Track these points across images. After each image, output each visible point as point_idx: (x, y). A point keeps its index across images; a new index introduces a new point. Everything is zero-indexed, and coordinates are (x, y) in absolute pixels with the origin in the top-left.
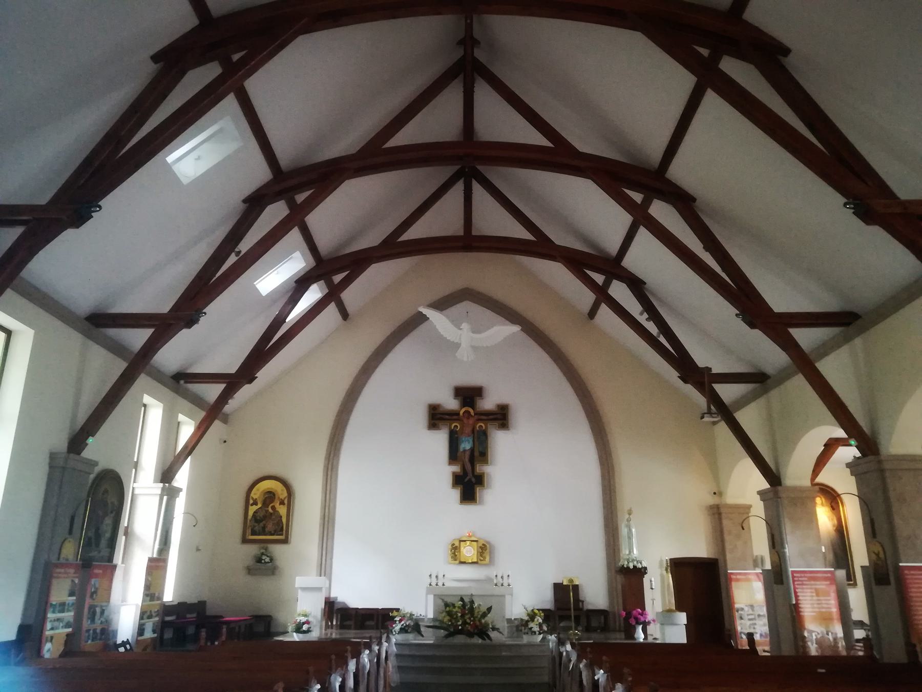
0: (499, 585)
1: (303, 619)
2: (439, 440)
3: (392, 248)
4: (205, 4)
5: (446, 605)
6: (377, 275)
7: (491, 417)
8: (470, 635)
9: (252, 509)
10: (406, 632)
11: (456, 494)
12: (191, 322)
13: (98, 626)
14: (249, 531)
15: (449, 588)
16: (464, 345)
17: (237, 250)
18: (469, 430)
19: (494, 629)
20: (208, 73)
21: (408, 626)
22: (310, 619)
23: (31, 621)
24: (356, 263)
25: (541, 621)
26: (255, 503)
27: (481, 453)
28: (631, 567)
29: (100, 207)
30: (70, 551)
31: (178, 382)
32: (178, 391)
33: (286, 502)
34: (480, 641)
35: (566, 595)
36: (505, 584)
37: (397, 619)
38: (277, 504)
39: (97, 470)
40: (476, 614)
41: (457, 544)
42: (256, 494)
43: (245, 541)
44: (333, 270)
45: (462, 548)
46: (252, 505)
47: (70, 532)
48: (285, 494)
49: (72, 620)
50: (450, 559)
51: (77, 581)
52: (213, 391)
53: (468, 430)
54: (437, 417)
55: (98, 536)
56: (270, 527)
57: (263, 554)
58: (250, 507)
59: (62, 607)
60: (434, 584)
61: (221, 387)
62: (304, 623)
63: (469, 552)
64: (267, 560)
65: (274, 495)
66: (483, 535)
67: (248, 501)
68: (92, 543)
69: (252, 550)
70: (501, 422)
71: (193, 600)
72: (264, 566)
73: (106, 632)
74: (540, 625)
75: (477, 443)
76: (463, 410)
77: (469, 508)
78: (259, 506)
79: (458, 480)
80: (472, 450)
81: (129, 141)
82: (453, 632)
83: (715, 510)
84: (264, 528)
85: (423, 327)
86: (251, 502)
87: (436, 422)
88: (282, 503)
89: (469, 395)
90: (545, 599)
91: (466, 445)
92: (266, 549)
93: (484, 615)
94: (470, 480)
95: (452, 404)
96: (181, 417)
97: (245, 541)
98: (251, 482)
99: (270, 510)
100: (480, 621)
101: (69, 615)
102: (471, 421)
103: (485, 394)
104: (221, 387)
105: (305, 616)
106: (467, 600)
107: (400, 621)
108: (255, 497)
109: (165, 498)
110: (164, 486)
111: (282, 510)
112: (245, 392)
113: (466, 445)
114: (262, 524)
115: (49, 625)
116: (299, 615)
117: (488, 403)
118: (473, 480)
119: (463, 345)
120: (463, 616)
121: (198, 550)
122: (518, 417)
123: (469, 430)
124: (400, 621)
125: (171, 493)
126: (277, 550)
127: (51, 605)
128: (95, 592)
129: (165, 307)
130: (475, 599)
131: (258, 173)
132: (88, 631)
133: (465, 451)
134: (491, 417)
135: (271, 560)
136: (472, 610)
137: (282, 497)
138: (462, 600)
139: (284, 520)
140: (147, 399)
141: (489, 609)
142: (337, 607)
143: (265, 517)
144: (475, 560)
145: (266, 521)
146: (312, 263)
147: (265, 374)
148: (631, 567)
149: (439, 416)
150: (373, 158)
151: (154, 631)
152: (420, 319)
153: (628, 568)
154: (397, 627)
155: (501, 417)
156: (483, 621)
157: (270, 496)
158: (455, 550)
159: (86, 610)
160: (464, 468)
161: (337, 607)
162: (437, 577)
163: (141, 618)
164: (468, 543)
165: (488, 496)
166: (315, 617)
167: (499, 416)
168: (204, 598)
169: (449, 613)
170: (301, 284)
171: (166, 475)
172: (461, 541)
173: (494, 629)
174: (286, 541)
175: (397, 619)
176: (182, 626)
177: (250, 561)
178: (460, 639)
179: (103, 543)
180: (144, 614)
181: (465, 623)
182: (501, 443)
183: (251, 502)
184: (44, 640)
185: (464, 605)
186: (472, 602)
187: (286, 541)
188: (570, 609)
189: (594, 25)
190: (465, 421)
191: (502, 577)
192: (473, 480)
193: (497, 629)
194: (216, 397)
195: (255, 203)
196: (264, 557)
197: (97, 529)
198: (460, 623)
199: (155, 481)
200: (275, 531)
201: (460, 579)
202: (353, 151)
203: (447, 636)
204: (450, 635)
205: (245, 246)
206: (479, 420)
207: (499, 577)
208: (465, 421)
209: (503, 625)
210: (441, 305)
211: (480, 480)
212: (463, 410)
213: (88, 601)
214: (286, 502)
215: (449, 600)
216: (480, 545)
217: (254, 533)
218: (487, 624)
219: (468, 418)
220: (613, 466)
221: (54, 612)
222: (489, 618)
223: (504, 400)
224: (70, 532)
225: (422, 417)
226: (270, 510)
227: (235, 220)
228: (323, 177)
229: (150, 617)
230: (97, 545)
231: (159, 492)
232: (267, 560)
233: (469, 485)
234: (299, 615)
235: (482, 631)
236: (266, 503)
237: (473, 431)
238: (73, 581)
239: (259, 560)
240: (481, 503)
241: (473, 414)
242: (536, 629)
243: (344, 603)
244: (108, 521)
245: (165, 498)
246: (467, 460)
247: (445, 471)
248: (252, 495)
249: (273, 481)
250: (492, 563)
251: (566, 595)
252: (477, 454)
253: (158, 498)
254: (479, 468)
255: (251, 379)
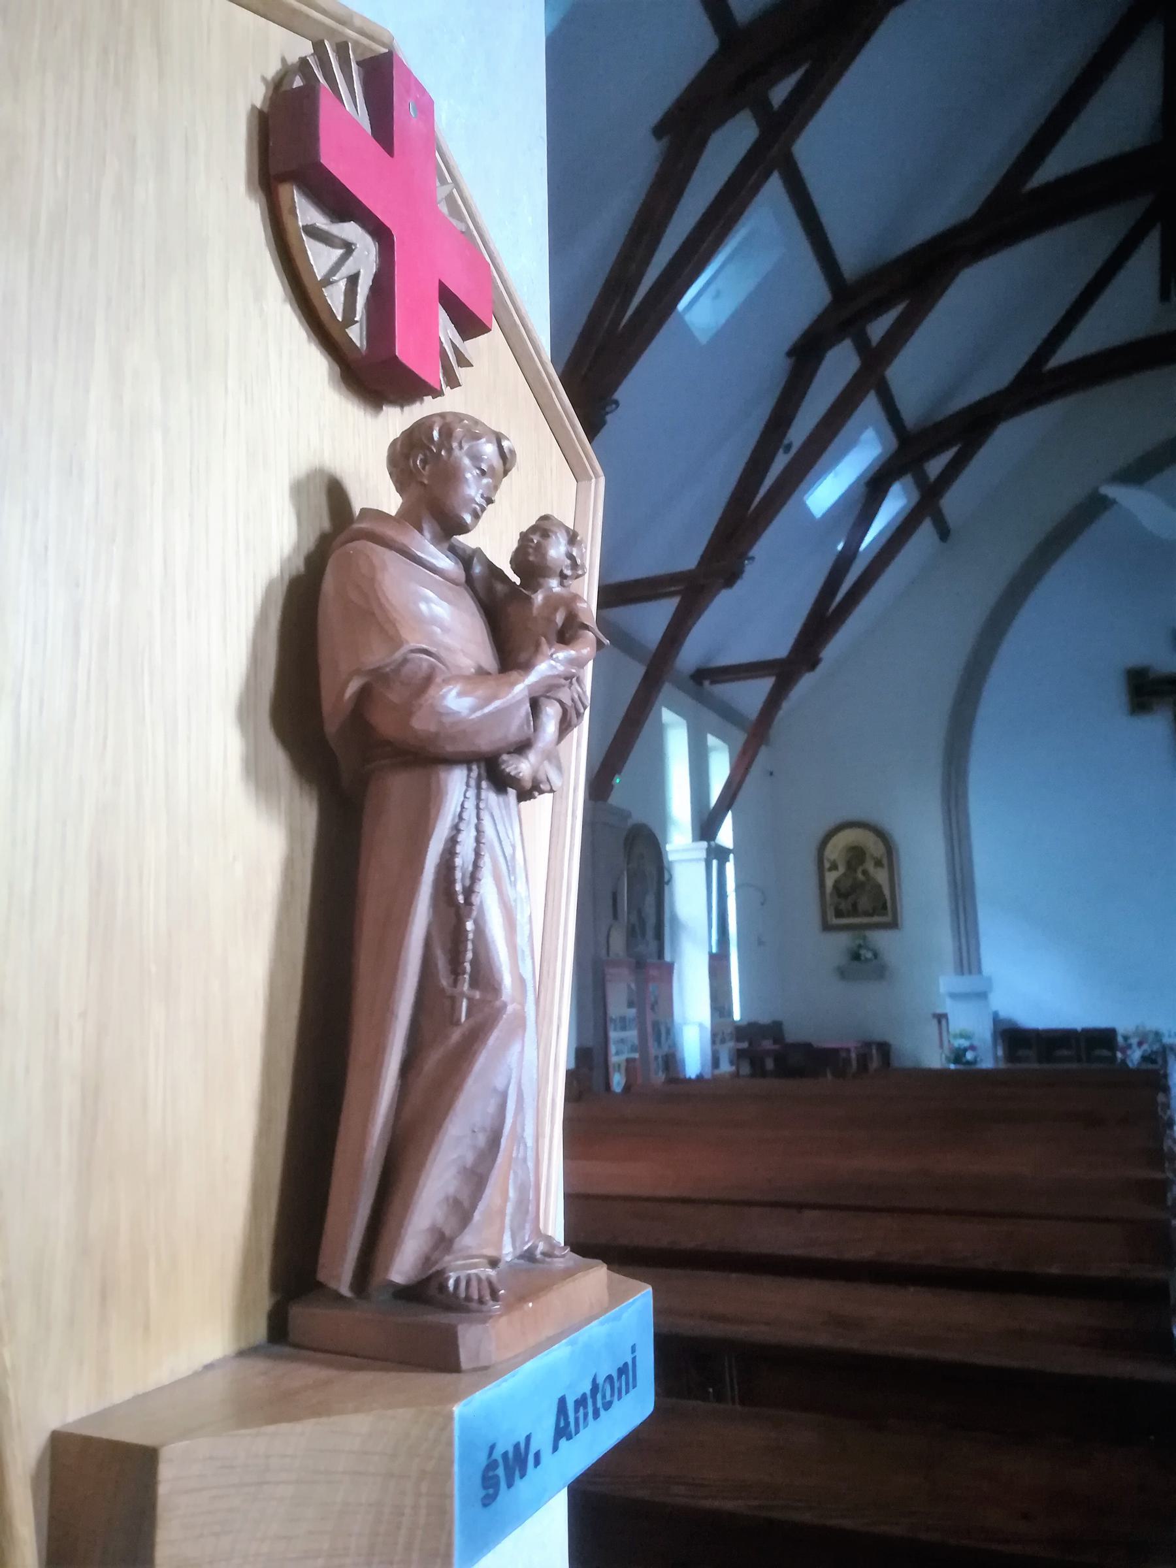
1: (964, 1043)
3: (1035, 385)
4: (727, 7)
6: (1009, 439)
9: (831, 878)
12: (731, 577)
13: (665, 1049)
14: (831, 913)
17: (786, 442)
20: (734, 139)
22: (976, 1043)
23: (590, 1043)
24: (971, 427)
26: (834, 867)
29: (617, 403)
30: (618, 942)
31: (701, 684)
32: (702, 698)
33: (885, 861)
39: (630, 822)
42: (836, 849)
43: (827, 927)
44: (926, 452)
46: (830, 869)
47: (615, 916)
49: (636, 1042)
51: (633, 986)
52: (751, 695)
55: (642, 921)
56: (864, 902)
57: (860, 946)
59: (623, 1024)
61: (764, 686)
62: (965, 1050)
64: (869, 955)
68: (634, 933)
69: (842, 941)
71: (765, 1019)
72: (862, 964)
73: (671, 1061)
81: (639, 282)
84: (855, 905)
85: (1106, 520)
88: (878, 863)
92: (865, 938)
96: (712, 740)
97: (827, 927)
98: (820, 834)
99: (860, 876)
101: (632, 1034)
104: (764, 686)
107: (1140, 1044)
109: (715, 863)
110: (709, 845)
111: (881, 876)
112: (806, 683)
115: (613, 1049)
116: (955, 1037)
121: (760, 943)
124: (1140, 1044)
125: (718, 854)
126: (881, 939)
127: (611, 1019)
128: (656, 1002)
129: (688, 560)
131: (810, 296)
132: (656, 1058)
135: (876, 955)
139: (887, 892)
140: (667, 716)
145: (857, 894)
146: (893, 443)
147: (831, 652)
150: (1008, 215)
151: (732, 1063)
152: (1094, 507)
157: (856, 855)
159: (649, 1029)
163: (713, 1042)
168: (778, 1017)
170: (874, 488)
171: (706, 828)
174: (894, 925)
176: (766, 1054)
179: (650, 933)
180: (717, 1037)
183: (827, 865)
184: (611, 1069)
187: (894, 925)
194: (762, 704)
195: (806, 354)
196: (863, 952)
197: (640, 912)
199: (694, 840)
202: (968, 212)
205: (799, 432)
210: (1138, 472)
213: (650, 1017)
214: (885, 861)
217: (839, 914)
221: (615, 1030)
224: (615, 916)
225: (1116, 693)
226: (860, 876)
227: (777, 393)
228: (919, 275)
229: (723, 1041)
230: (644, 934)
231: (703, 855)
232: (869, 955)
234: (955, 1037)
238: (629, 986)
239: (856, 957)
243: (1010, 1021)
244: (650, 900)
245: (715, 863)
253: (703, 865)
255: (813, 663)
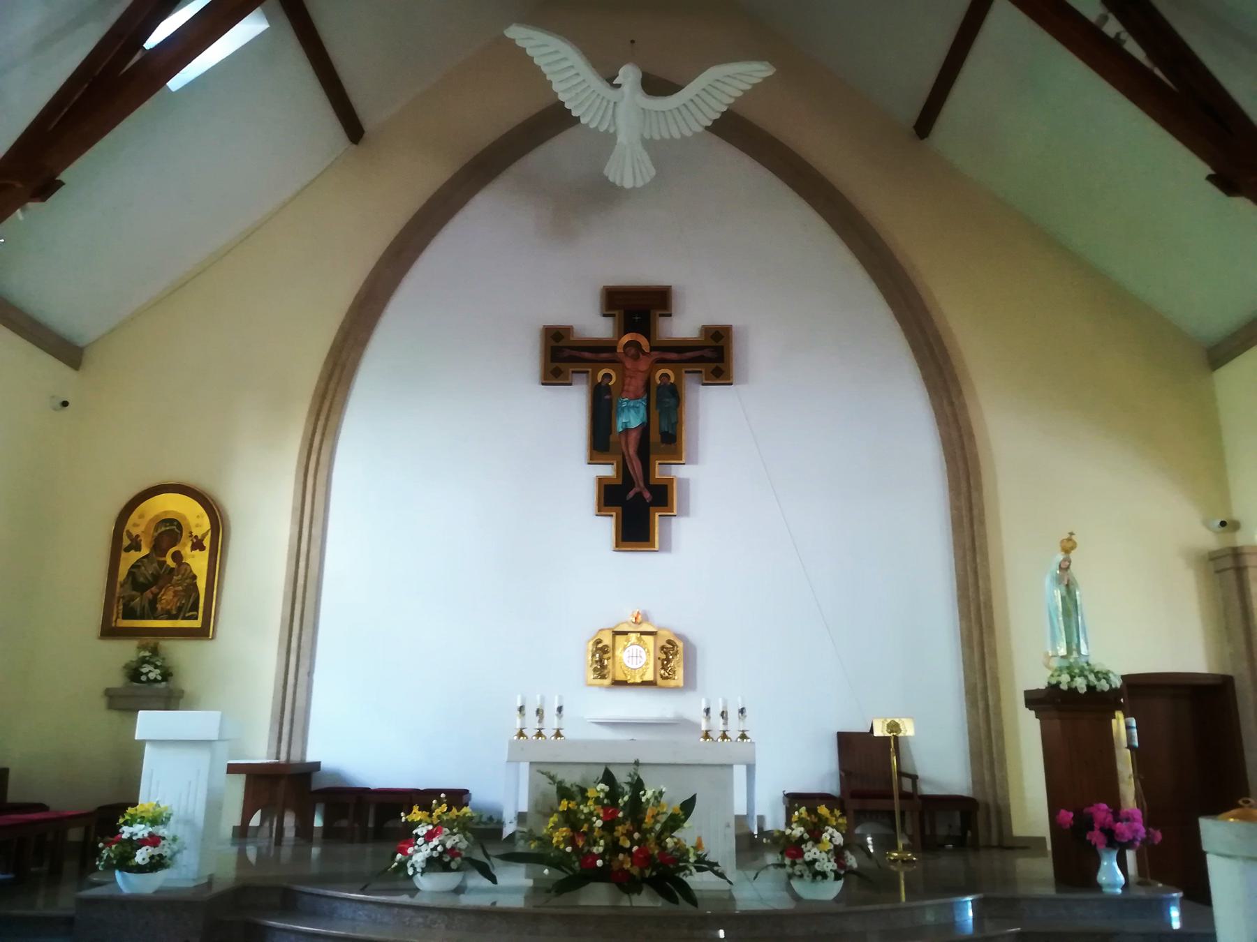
0: (716, 735)
2: (570, 407)
5: (564, 792)
7: (689, 355)
8: (628, 884)
9: (129, 559)
10: (446, 868)
11: (607, 527)
15: (574, 744)
16: (627, 136)
18: (637, 393)
19: (704, 864)
21: (453, 852)
25: (839, 839)
26: (135, 546)
27: (666, 436)
28: (1083, 689)
33: (207, 543)
34: (660, 903)
35: (867, 763)
36: (734, 734)
37: (422, 830)
38: (186, 550)
40: (648, 821)
41: (607, 640)
43: (109, 631)
45: (618, 653)
46: (128, 549)
48: (206, 524)
50: (591, 675)
53: (637, 383)
54: (561, 356)
56: (168, 598)
57: (144, 661)
58: (124, 555)
60: (530, 733)
62: (142, 843)
63: (635, 658)
65: (179, 526)
66: (668, 620)
67: (120, 541)
69: (127, 650)
70: (713, 366)
74: (838, 853)
75: (655, 413)
76: (626, 339)
77: (637, 561)
78: (145, 551)
79: (609, 496)
80: (645, 429)
82: (573, 871)
83: (1229, 563)
84: (154, 601)
86: (126, 542)
87: (562, 366)
88: (198, 545)
89: (637, 307)
90: (818, 771)
91: (630, 418)
92: (155, 651)
93: (674, 823)
94: (639, 495)
95: (594, 325)
97: (109, 631)
99: (170, 562)
100: (660, 839)
102: (643, 365)
103: (676, 303)
105: (154, 822)
106: (622, 777)
107: (429, 837)
108: (135, 532)
111: (198, 562)
113: (630, 418)
114: (148, 594)
117: (683, 325)
118: (647, 495)
119: (622, 138)
120: (609, 826)
122: (756, 353)
123: (637, 393)
124: (429, 837)
126: (180, 652)
130: (644, 775)
133: (627, 431)
134: (689, 355)
135: (166, 675)
136: (636, 806)
137: (198, 532)
138: (608, 778)
139: (202, 584)
141: (688, 806)
142: (317, 784)
143: (156, 578)
144: (649, 677)
148: (1083, 689)
149: (567, 353)
153: (1073, 691)
154: (419, 855)
155: (714, 356)
156: (670, 842)
158: (602, 655)
160: (624, 470)
161: (317, 784)
162: (539, 712)
164: (633, 637)
165: (688, 531)
166: (188, 822)
167: (708, 353)
169: (570, 819)
172: (616, 633)
173: (704, 864)
175: (422, 830)
177: (117, 680)
178: (598, 896)
181: (614, 848)
182: (712, 411)
183: (126, 542)
185: (614, 794)
186: (638, 785)
187: (203, 633)
188: (891, 797)
189: (786, 187)
190: (629, 364)
191: (723, 714)
192: (647, 495)
193: (712, 866)
198: (598, 850)
200: (180, 609)
201: (596, 722)
203: (563, 887)
204: (563, 887)
206: (663, 362)
207: (715, 713)
208: (629, 364)
209: (721, 848)
211: (662, 496)
212: (626, 339)
214: (207, 543)
215: (571, 778)
216: (662, 642)
217: (129, 614)
218: (682, 853)
219: (636, 358)
220: (976, 457)
222: (687, 835)
223: (718, 319)
225: (530, 358)
226: (170, 562)
233: (637, 508)
235: (665, 872)
236: (159, 546)
237: (648, 385)
239: (134, 674)
240: (666, 547)
241: (647, 350)
242: (829, 866)
246: (632, 450)
247: (585, 478)
248: (129, 526)
249: (199, 509)
250: (690, 683)
251: (867, 763)
252: (655, 437)
254: (660, 472)
